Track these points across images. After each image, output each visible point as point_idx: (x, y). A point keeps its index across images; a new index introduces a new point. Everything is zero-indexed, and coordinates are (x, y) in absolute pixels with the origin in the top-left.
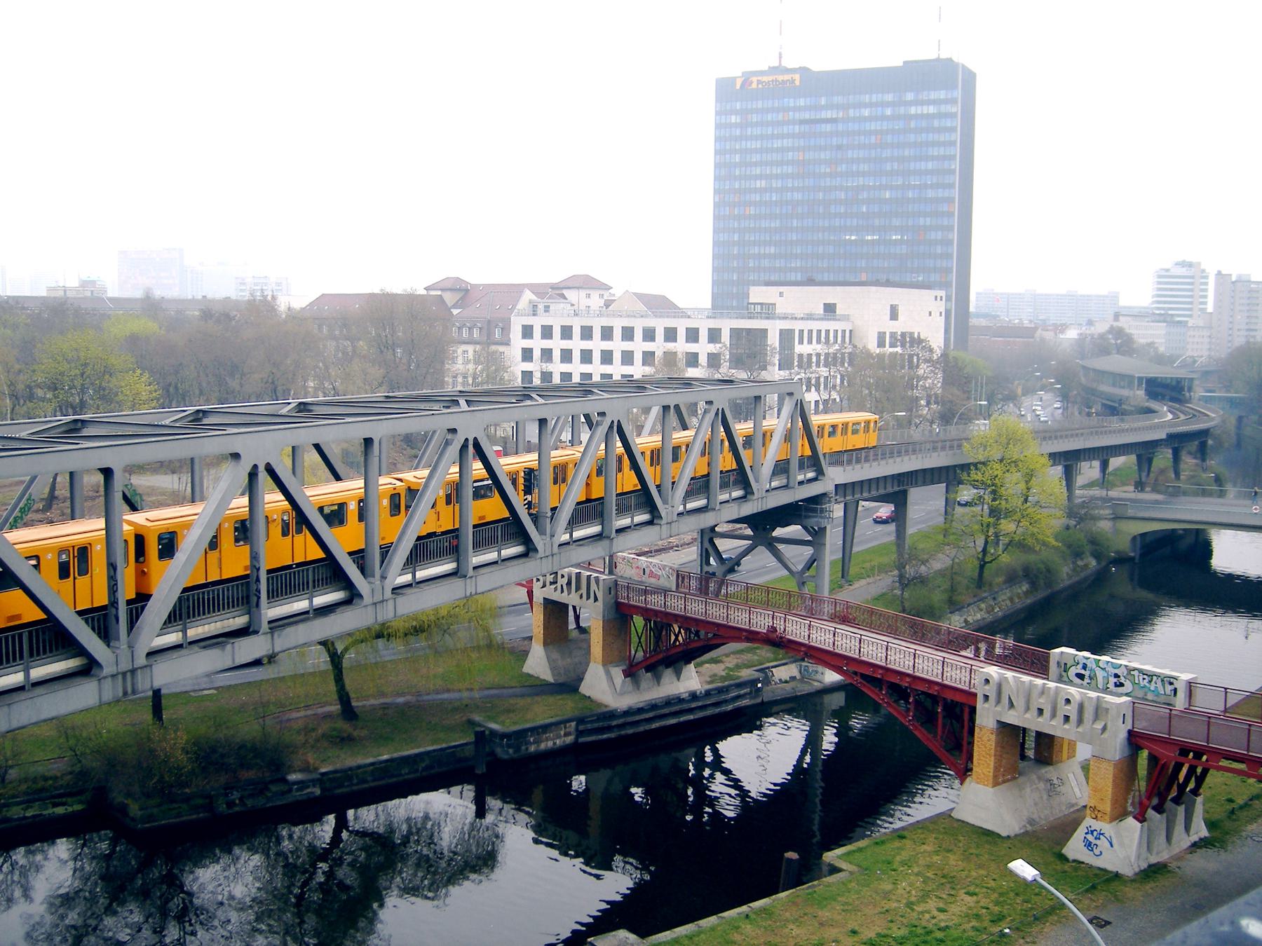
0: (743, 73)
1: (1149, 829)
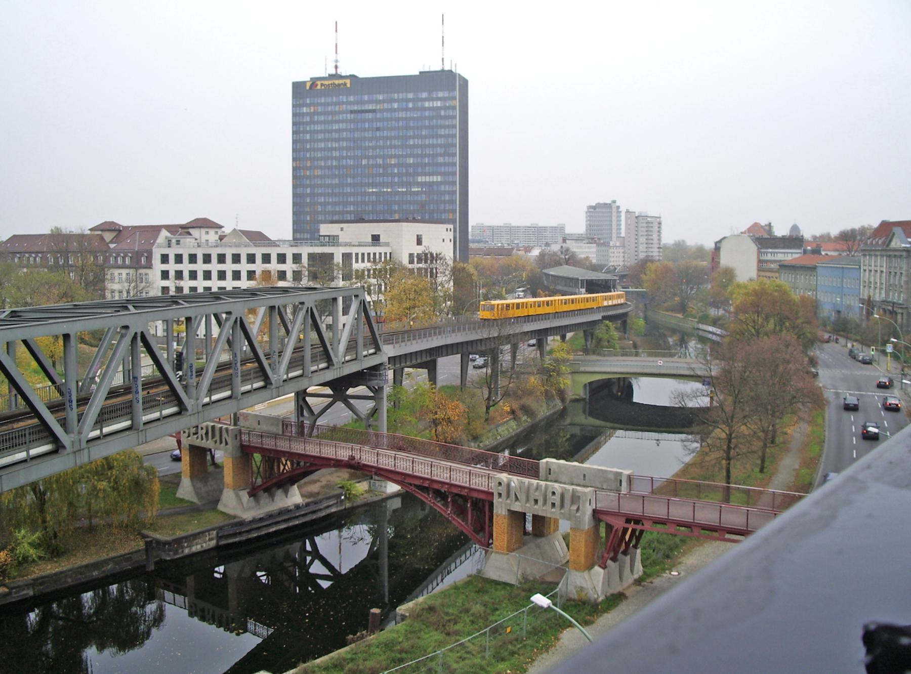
1: (608, 573)
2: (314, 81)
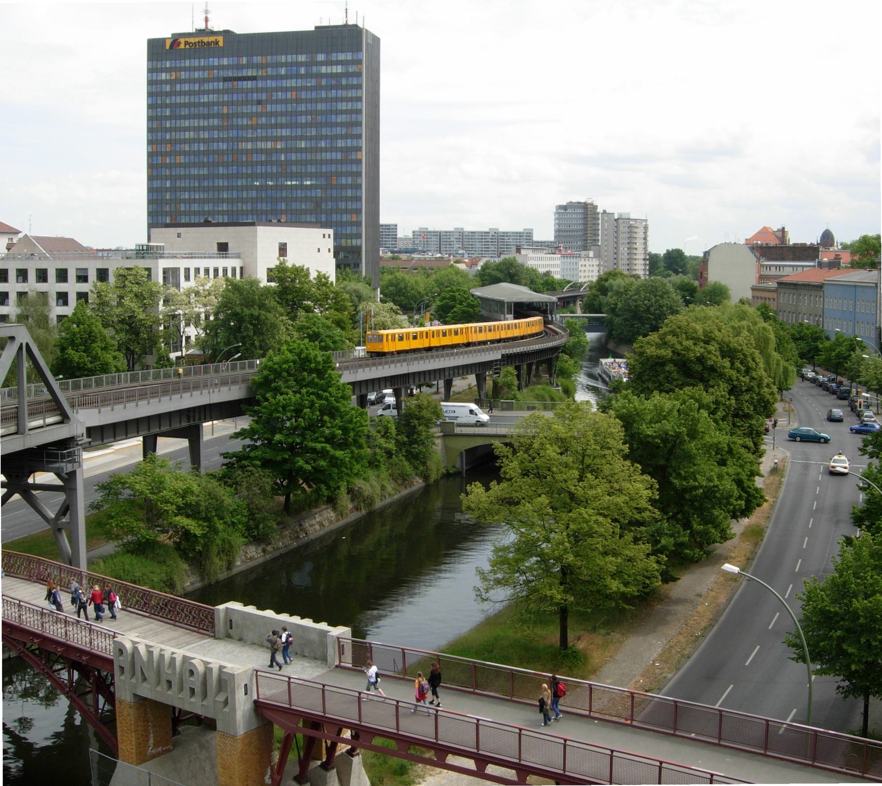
0: (172, 35)
2: (176, 39)
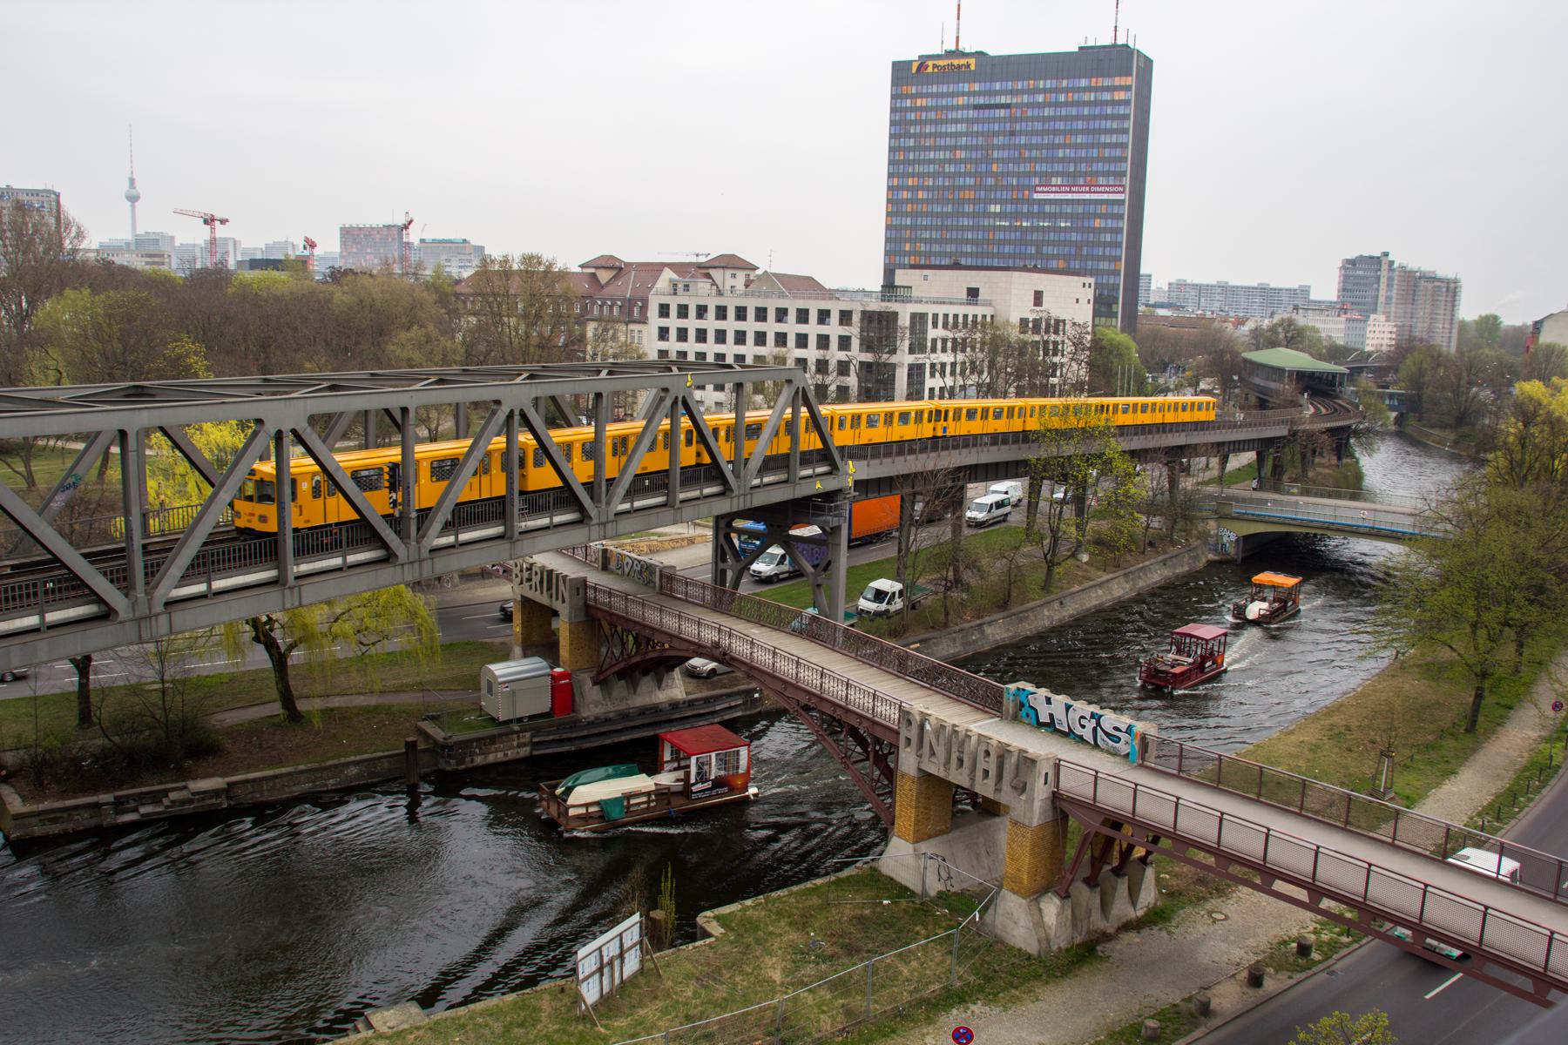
2: (923, 60)
